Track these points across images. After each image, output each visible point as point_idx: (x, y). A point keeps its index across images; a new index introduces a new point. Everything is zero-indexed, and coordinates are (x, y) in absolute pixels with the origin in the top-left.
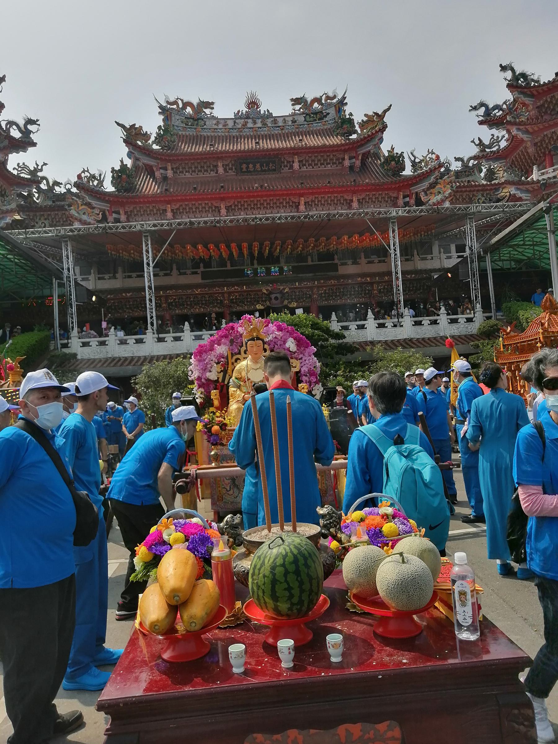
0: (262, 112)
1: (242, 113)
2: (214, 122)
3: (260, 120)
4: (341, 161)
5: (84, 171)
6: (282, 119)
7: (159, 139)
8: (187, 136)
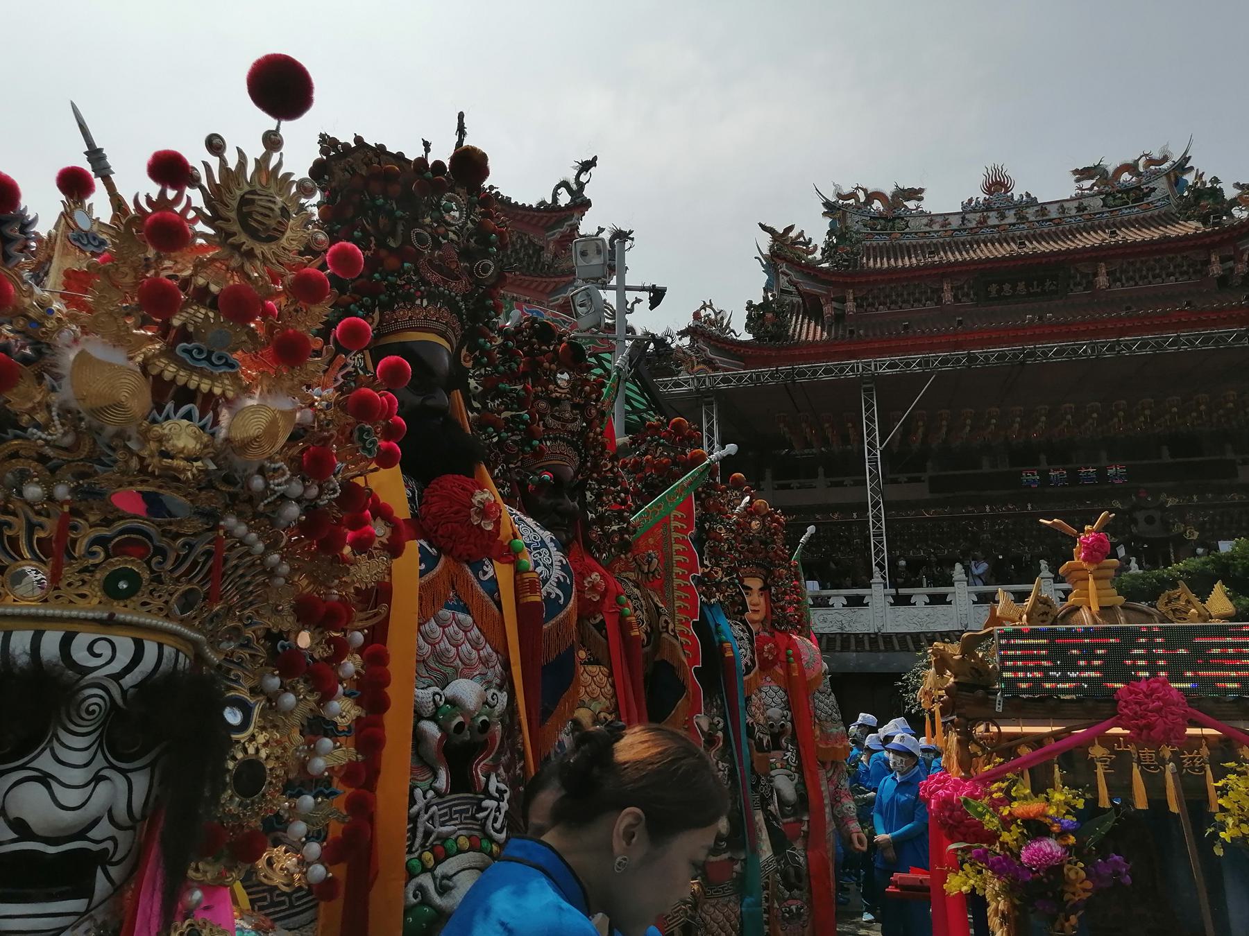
0: (1016, 198)
1: (978, 202)
2: (925, 221)
3: (1013, 212)
4: (1199, 267)
5: (704, 307)
6: (1056, 206)
7: (829, 250)
8: (874, 248)
